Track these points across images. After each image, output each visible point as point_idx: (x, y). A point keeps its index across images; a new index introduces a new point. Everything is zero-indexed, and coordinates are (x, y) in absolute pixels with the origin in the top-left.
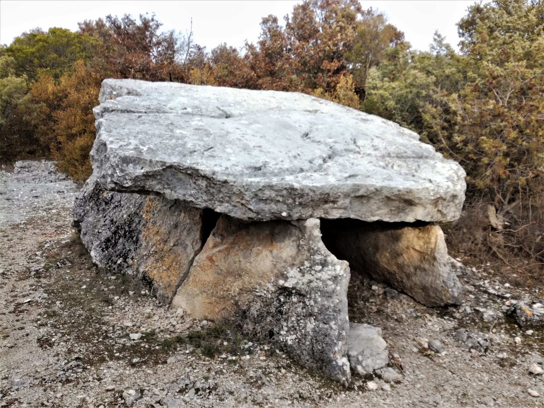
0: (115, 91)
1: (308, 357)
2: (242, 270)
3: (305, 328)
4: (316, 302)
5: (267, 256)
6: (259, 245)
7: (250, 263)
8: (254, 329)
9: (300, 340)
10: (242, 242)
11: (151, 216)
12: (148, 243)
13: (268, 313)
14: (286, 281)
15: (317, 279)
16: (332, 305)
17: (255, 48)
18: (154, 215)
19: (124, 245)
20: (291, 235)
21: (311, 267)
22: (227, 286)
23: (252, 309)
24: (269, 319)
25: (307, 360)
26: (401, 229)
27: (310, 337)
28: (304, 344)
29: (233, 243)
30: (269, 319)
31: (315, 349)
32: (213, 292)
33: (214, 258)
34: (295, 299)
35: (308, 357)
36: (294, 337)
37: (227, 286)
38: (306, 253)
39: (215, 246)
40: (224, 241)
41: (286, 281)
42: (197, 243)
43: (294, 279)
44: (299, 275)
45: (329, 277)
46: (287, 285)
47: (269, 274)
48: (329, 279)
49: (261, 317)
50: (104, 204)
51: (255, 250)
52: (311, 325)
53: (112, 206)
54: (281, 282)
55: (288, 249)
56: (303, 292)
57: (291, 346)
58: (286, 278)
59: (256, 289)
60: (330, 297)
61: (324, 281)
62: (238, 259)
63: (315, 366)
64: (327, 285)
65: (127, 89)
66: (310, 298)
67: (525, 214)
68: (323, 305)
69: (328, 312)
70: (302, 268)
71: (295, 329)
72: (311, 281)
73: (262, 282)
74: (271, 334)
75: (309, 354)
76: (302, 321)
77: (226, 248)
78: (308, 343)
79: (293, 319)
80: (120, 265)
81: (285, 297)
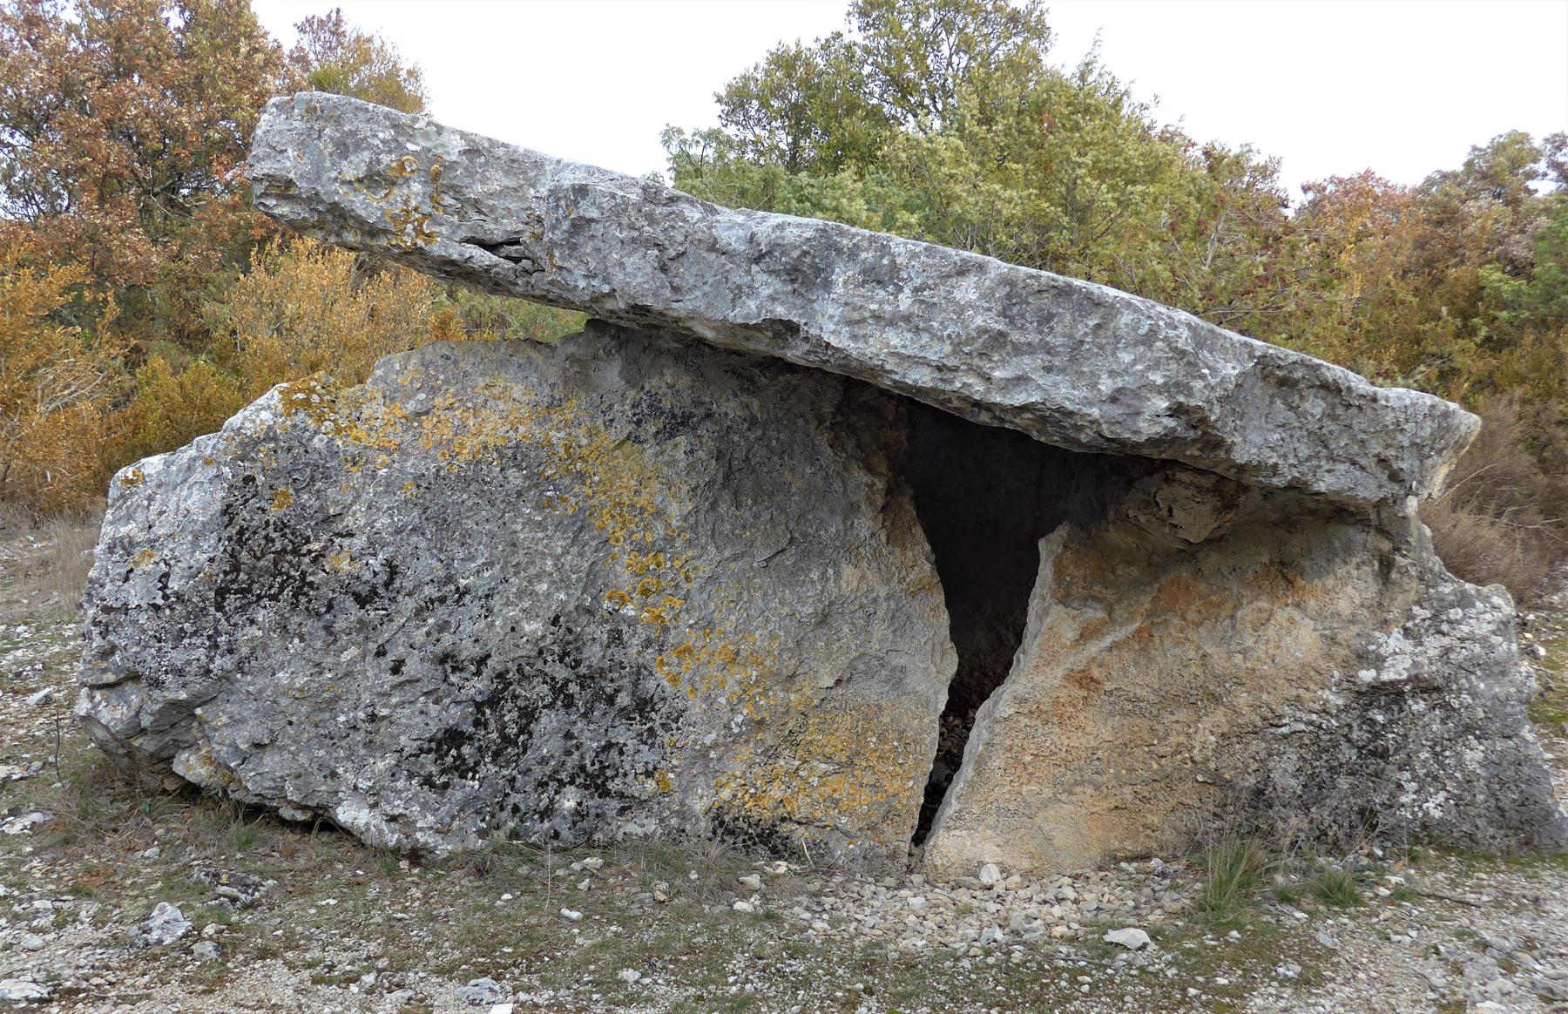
0: (411, 138)
1: (1491, 831)
2: (1220, 679)
3: (1461, 764)
4: (1474, 694)
5: (1292, 620)
6: (1257, 598)
7: (1244, 652)
8: (1311, 822)
9: (1459, 798)
10: (1189, 604)
11: (678, 604)
12: (709, 700)
13: (1331, 769)
14: (1379, 669)
15: (1462, 640)
16: (1512, 690)
17: (1091, 71)
18: (686, 598)
19: (568, 736)
20: (1349, 551)
21: (1434, 617)
22: (1173, 740)
23: (1275, 775)
24: (1344, 783)
25: (1493, 837)
26: (922, 517)
27: (1482, 782)
28: (1472, 803)
29: (1150, 614)
30: (1344, 783)
31: (1506, 804)
32: (1117, 776)
33: (1096, 673)
34: (1419, 706)
35: (1491, 831)
36: (1441, 796)
37: (1173, 740)
38: (1415, 584)
39: (1085, 636)
40: (1119, 612)
41: (1379, 669)
42: (944, 653)
43: (1400, 658)
44: (1408, 646)
45: (1492, 627)
46: (1386, 676)
47: (1323, 665)
48: (1494, 633)
49: (1315, 789)
50: (349, 602)
51: (1246, 613)
52: (1474, 755)
53: (408, 605)
54: (1367, 675)
55: (1349, 589)
56: (1440, 682)
57: (1441, 822)
58: (1378, 661)
59: (1280, 717)
60: (1503, 673)
61: (1484, 640)
62: (1190, 649)
63: (1513, 842)
64: (1492, 648)
65: (463, 135)
66: (1460, 691)
67: (101, 296)
68: (1496, 697)
69: (1509, 710)
70: (1410, 624)
71: (1436, 778)
72: (1447, 651)
73: (1302, 692)
74: (1367, 816)
75: (1491, 822)
76: (1447, 753)
77: (1138, 631)
78: (1480, 797)
79: (1424, 755)
80: (579, 814)
81: (1387, 709)
